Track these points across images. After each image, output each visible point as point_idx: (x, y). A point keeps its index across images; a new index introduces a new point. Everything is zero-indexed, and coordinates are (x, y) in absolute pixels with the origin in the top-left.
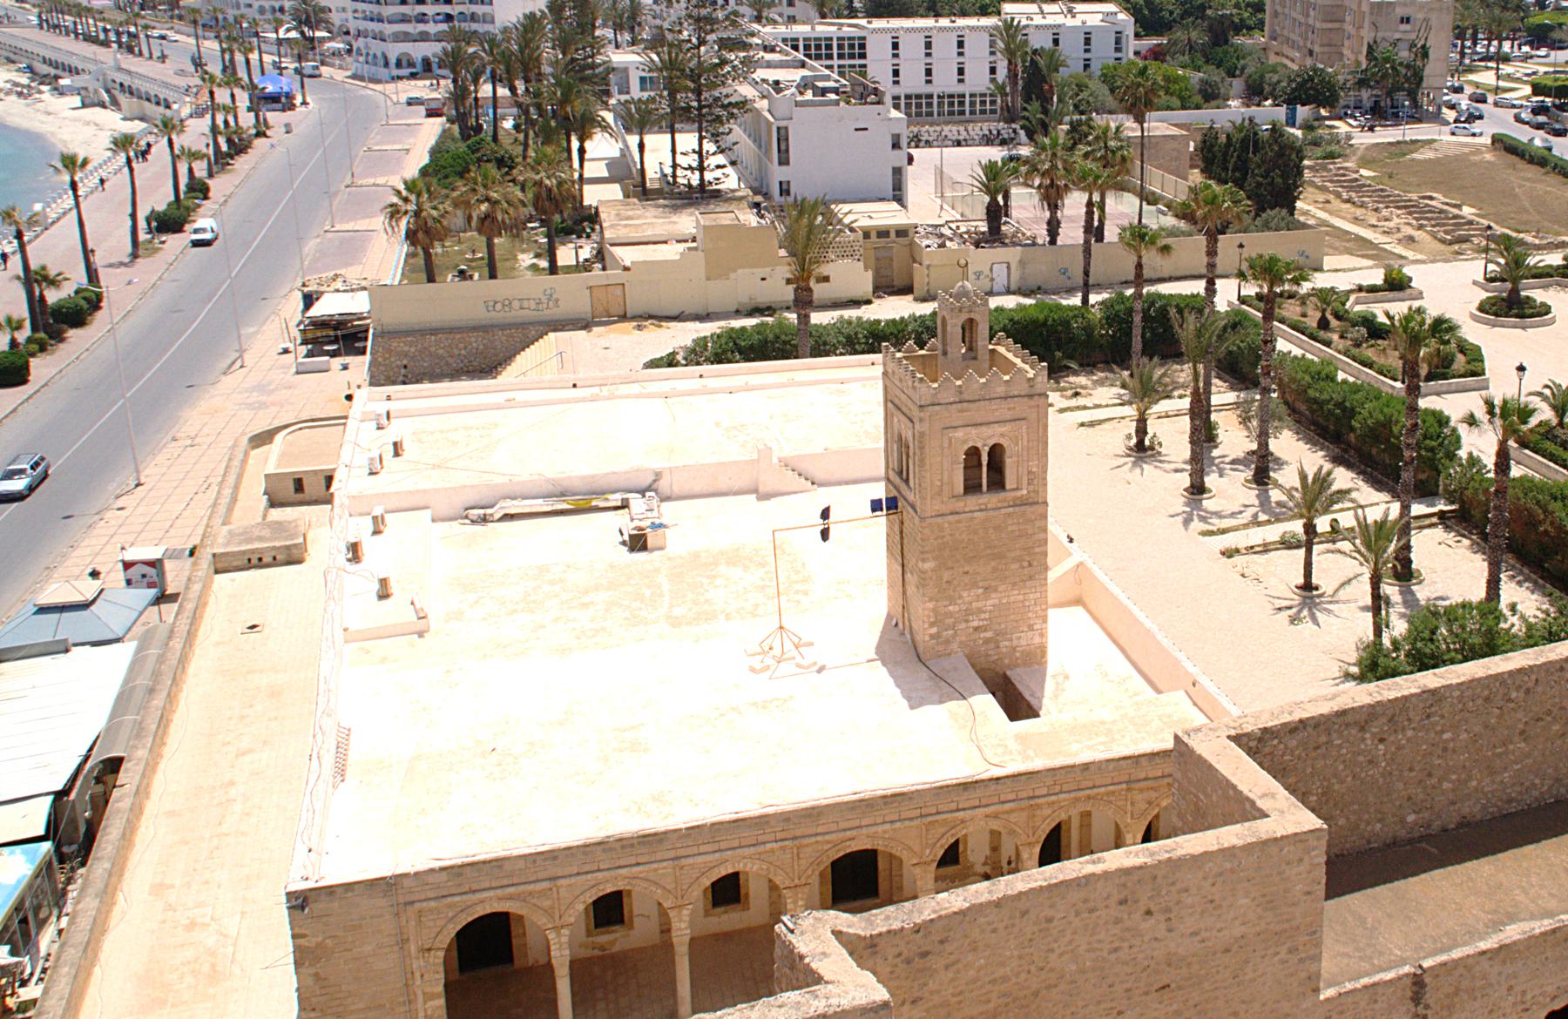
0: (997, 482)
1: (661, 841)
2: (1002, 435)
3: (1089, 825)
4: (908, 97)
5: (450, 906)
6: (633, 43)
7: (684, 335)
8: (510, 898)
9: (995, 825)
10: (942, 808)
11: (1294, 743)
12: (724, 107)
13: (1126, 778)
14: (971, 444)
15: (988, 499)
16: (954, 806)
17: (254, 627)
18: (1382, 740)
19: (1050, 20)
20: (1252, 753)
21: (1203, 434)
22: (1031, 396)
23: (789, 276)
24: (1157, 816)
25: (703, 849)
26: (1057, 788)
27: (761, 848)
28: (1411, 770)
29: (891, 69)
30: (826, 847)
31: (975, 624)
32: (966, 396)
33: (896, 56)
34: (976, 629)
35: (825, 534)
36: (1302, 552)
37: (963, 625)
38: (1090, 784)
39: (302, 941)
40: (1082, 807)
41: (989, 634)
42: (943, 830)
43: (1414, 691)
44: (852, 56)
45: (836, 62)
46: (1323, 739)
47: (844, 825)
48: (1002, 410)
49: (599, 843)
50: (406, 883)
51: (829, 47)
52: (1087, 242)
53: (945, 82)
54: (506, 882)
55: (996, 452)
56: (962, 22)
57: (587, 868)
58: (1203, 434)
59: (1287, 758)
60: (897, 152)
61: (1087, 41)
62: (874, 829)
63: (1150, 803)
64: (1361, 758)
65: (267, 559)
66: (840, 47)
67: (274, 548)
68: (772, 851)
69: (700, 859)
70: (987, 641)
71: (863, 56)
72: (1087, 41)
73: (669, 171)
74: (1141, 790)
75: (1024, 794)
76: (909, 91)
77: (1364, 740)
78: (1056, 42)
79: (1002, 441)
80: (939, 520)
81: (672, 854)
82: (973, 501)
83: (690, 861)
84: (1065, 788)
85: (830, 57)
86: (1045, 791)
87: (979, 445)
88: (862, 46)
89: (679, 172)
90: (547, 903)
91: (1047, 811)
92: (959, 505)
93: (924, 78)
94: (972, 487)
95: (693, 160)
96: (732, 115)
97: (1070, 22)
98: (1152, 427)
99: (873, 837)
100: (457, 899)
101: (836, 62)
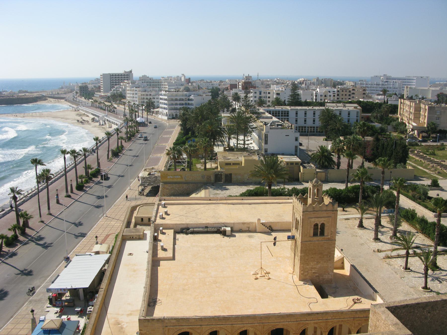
0: (322, 234)
1: (228, 319)
2: (324, 221)
3: (341, 329)
4: (299, 127)
5: (176, 328)
6: (228, 111)
7: (244, 189)
8: (190, 328)
9: (316, 326)
10: (302, 319)
11: (404, 311)
12: (252, 128)
13: (353, 317)
14: (316, 223)
15: (319, 238)
16: (305, 319)
17: (131, 254)
18: (429, 312)
19: (339, 108)
20: (392, 312)
21: (378, 223)
22: (333, 211)
23: (100, 138)
24: (360, 328)
25: (239, 323)
26: (334, 318)
27: (254, 324)
28: (437, 322)
29: (295, 120)
30: (271, 326)
31: (314, 271)
32: (315, 210)
33: (297, 116)
34: (314, 273)
35: (275, 244)
36: (405, 259)
37: (310, 272)
38: (343, 317)
39: (142, 332)
40: (340, 323)
41: (317, 275)
42: (302, 325)
43: (439, 300)
44: (285, 116)
45: (280, 117)
46: (412, 310)
47: (276, 321)
48: (325, 214)
49: (213, 318)
50: (166, 321)
51: (279, 113)
52: (348, 169)
53: (310, 123)
54: (190, 324)
55: (323, 225)
56: (315, 108)
57: (209, 324)
58: (378, 223)
59: (402, 315)
60: (296, 142)
61: (349, 114)
62: (283, 323)
63: (359, 324)
64: (423, 317)
65: (134, 238)
66: (282, 113)
67: (136, 235)
68: (257, 326)
69: (238, 325)
70: (316, 276)
71: (288, 116)
72: (349, 114)
73: (236, 145)
74: (357, 320)
75: (324, 318)
76: (300, 126)
77: (424, 312)
78: (340, 114)
79: (324, 222)
80: (306, 243)
81: (231, 323)
82: (316, 238)
83: (235, 325)
84: (336, 317)
85: (279, 116)
86: (330, 318)
87: (318, 223)
88: (288, 113)
89: (239, 145)
90: (199, 331)
91: (330, 323)
92: (311, 239)
93: (304, 122)
94: (315, 234)
95: (242, 142)
96: (253, 131)
97: (344, 109)
98: (364, 221)
99: (284, 325)
100: (178, 327)
101: (280, 117)
